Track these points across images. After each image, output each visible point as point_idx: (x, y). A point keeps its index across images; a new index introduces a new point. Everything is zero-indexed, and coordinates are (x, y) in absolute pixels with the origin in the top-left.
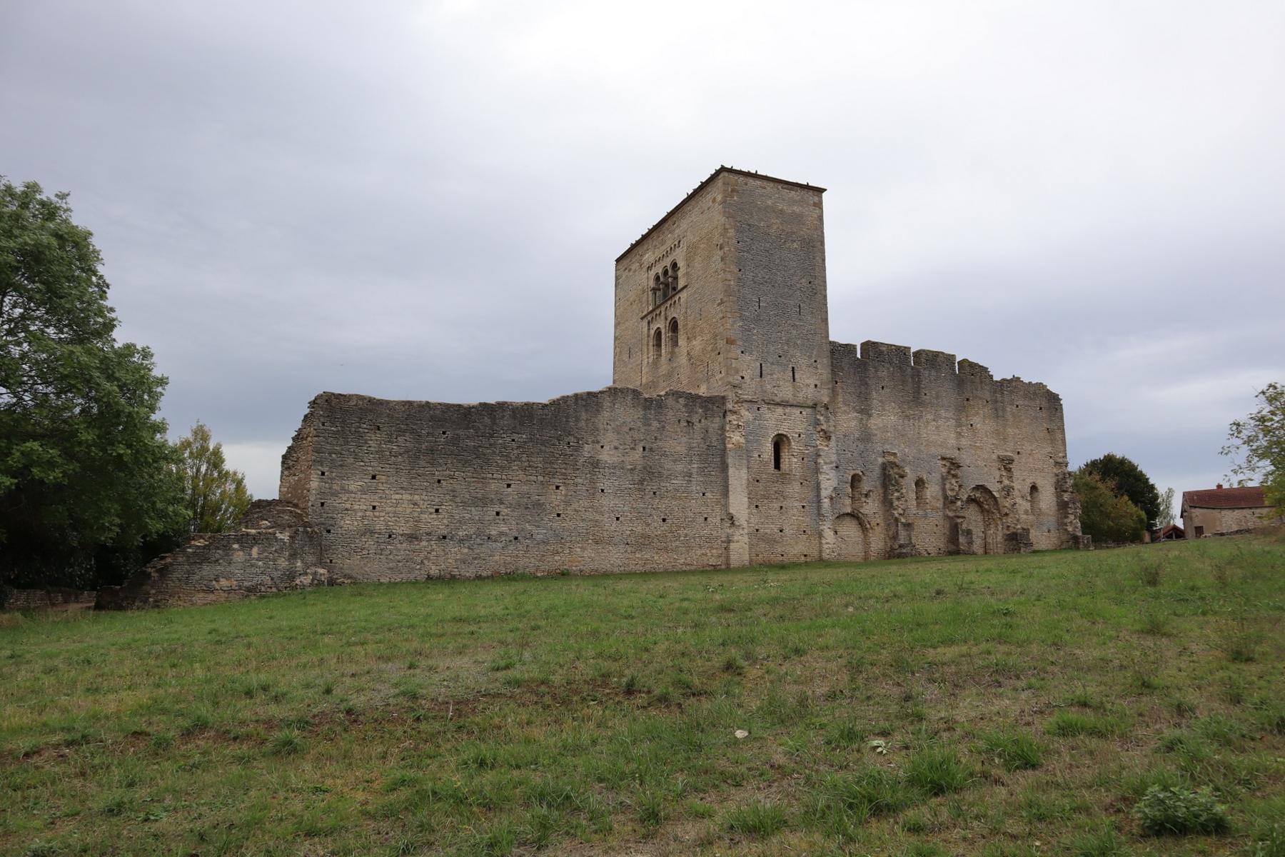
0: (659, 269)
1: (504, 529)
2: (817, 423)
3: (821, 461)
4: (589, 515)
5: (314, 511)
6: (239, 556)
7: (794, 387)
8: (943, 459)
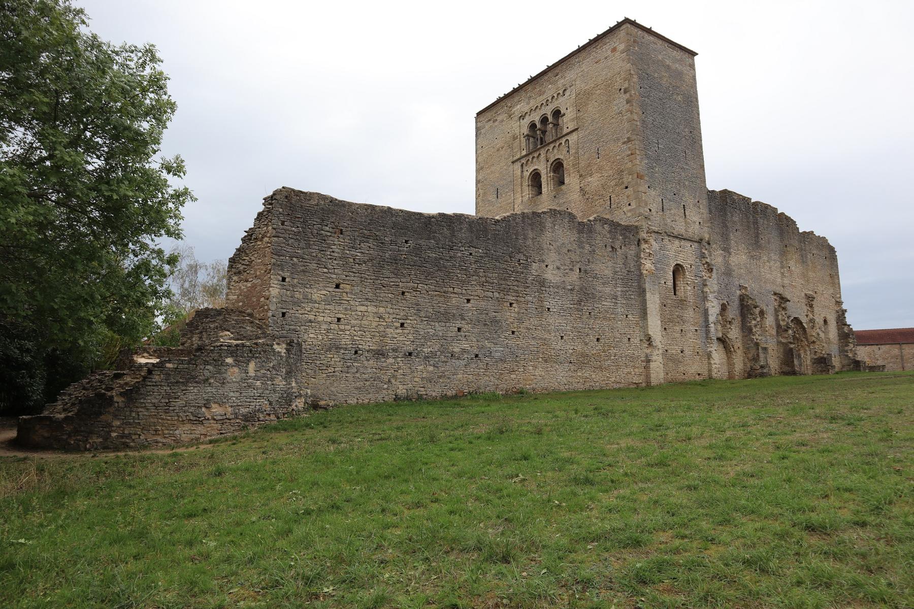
0: (536, 118)
1: (466, 346)
2: (703, 256)
3: (706, 289)
4: (537, 334)
5: (276, 322)
6: (234, 374)
7: (686, 222)
8: (775, 294)
